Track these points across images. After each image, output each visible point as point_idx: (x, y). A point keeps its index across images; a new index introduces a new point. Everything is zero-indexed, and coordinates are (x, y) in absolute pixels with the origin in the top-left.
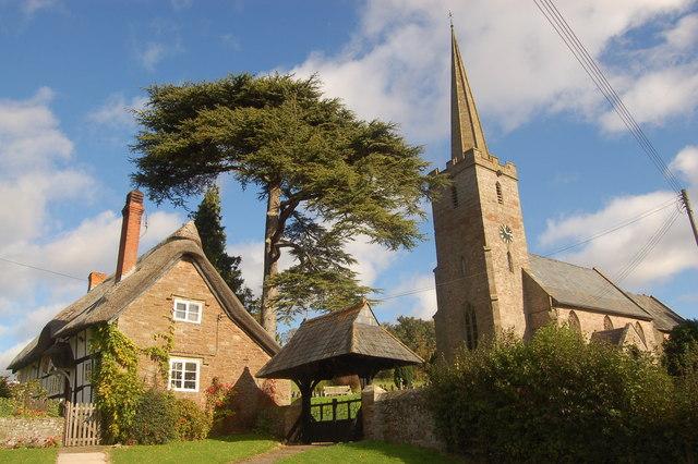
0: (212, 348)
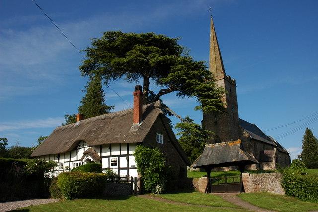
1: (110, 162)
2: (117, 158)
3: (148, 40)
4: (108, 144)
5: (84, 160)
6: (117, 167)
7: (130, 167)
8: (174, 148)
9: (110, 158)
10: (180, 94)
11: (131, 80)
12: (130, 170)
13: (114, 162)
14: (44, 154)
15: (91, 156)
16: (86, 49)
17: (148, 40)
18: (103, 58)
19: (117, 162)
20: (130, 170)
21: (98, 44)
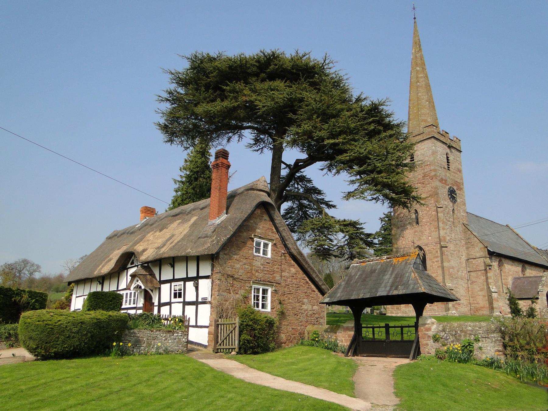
0: (278, 278)
1: (173, 292)
2: (182, 283)
3: (311, 80)
4: (208, 255)
5: (132, 288)
6: (181, 300)
7: (200, 300)
8: (296, 265)
9: (173, 284)
10: (330, 168)
11: (262, 148)
12: (200, 306)
13: (178, 292)
14: (83, 277)
15: (12, 298)
16: (166, 95)
17: (311, 80)
18: (367, 129)
19: (182, 291)
20: (200, 306)
21: (183, 82)
